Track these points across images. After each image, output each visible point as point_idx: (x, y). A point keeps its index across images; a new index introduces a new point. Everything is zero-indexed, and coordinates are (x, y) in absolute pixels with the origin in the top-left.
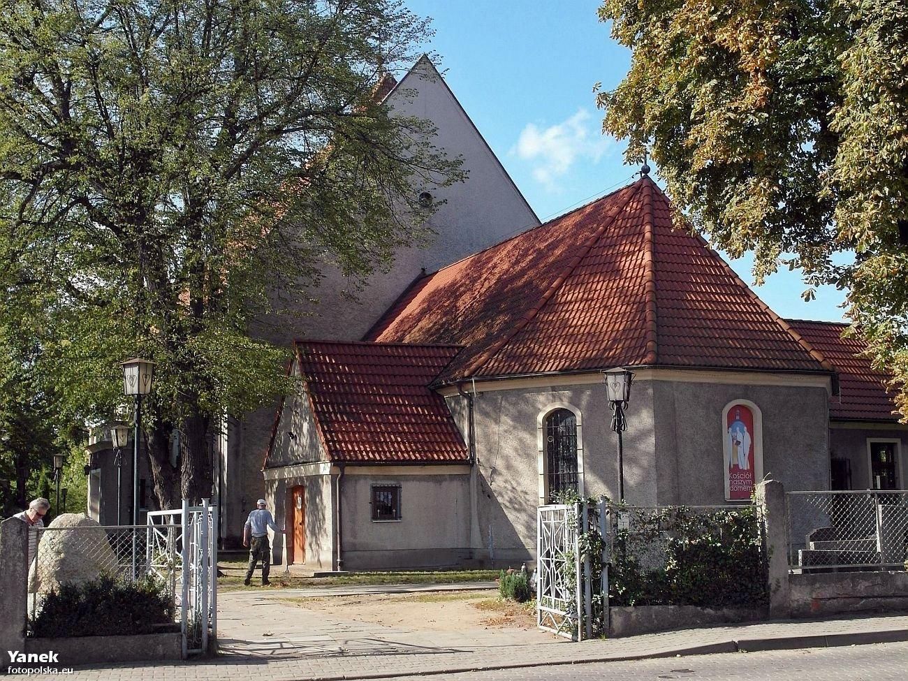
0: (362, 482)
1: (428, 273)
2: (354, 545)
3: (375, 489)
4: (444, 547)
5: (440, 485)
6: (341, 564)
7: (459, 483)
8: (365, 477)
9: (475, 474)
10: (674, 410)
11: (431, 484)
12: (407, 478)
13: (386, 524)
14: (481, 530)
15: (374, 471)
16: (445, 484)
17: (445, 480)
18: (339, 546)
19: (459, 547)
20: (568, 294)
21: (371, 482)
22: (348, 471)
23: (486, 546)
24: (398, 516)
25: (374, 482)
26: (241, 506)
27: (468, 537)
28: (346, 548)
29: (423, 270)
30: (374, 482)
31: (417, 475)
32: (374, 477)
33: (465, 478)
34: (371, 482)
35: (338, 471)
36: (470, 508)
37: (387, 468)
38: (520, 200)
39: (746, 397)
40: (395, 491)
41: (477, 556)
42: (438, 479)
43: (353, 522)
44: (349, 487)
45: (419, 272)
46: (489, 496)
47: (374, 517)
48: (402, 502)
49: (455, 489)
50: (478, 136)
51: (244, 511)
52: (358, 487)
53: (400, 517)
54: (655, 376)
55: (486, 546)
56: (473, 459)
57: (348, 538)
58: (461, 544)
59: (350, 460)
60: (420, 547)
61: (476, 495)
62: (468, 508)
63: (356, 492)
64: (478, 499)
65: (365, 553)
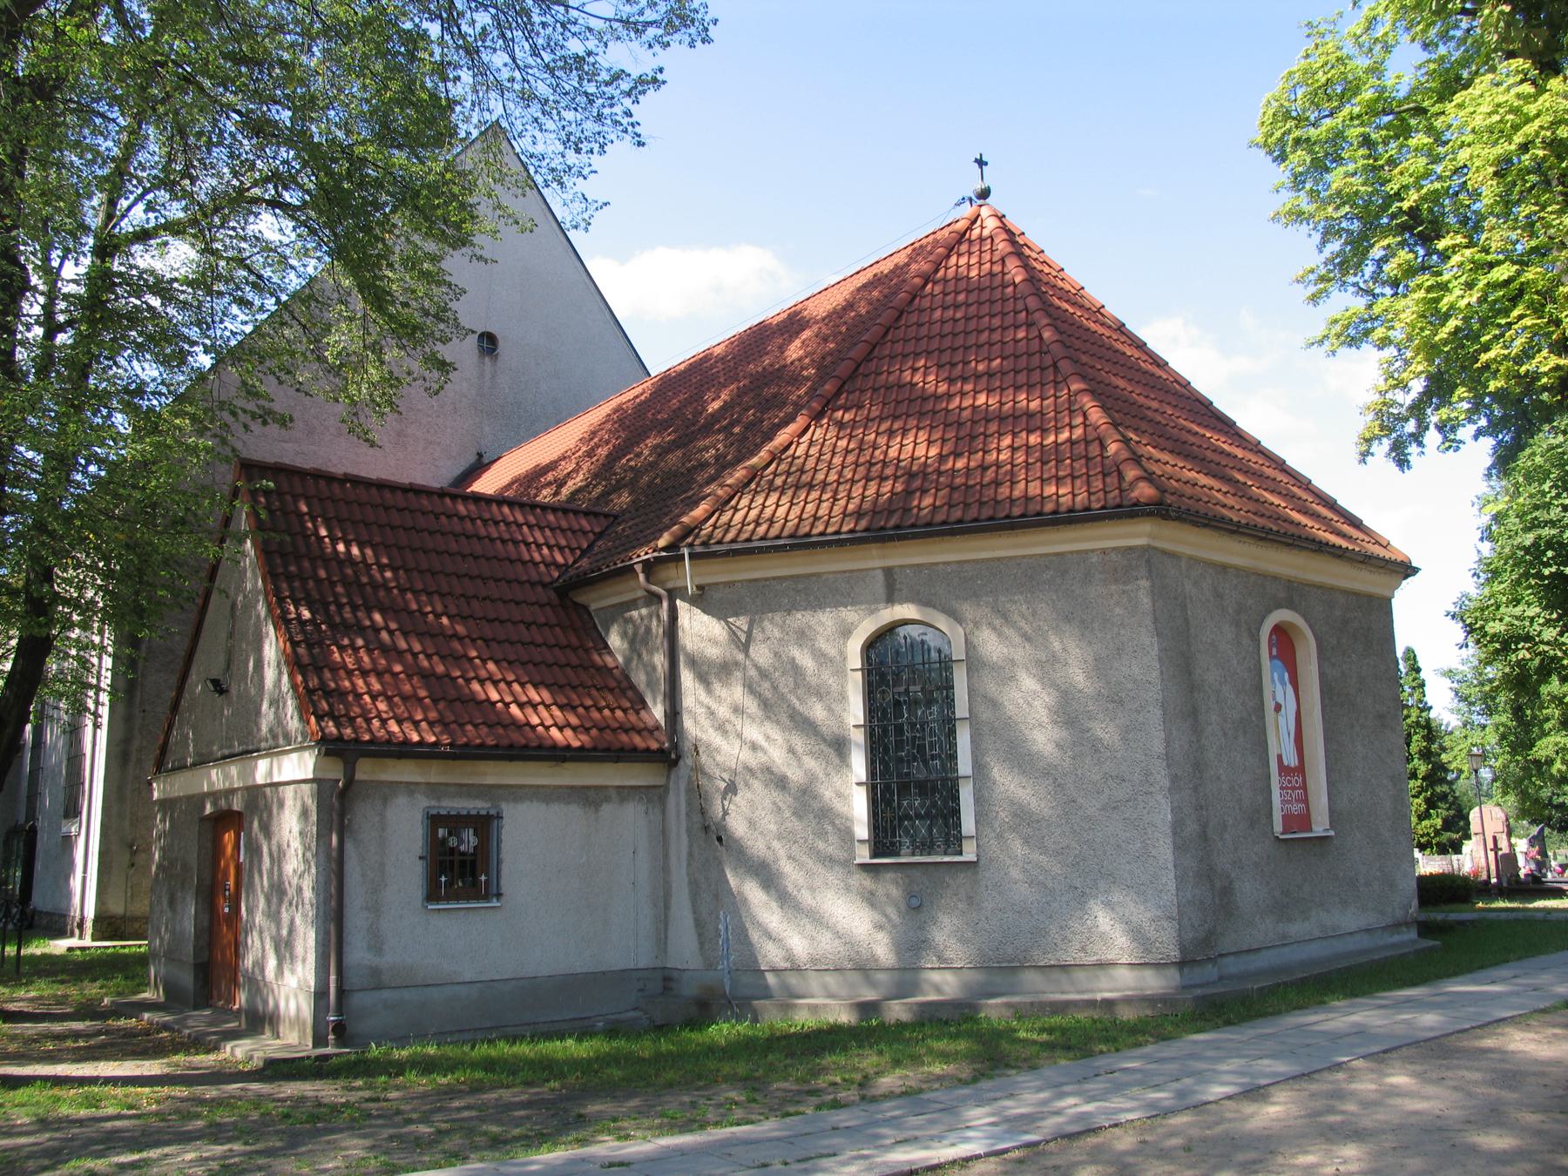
0: (401, 801)
1: (486, 460)
2: (375, 972)
3: (434, 820)
4: (603, 969)
5: (597, 811)
6: (339, 1029)
7: (641, 808)
8: (411, 788)
9: (683, 786)
10: (1187, 621)
11: (575, 811)
12: (517, 793)
13: (462, 913)
14: (699, 924)
15: (434, 773)
16: (607, 809)
17: (607, 799)
18: (333, 978)
19: (641, 966)
20: (799, 444)
21: (423, 802)
22: (366, 770)
23: (710, 965)
24: (490, 892)
25: (433, 803)
26: (127, 856)
27: (662, 940)
28: (353, 980)
29: (480, 455)
30: (433, 803)
31: (543, 786)
32: (433, 789)
33: (655, 796)
34: (423, 802)
35: (336, 772)
36: (666, 869)
37: (469, 766)
38: (636, 364)
39: (1290, 605)
40: (485, 824)
41: (689, 989)
42: (590, 797)
43: (375, 909)
44: (365, 815)
45: (472, 458)
46: (720, 839)
47: (433, 895)
48: (503, 855)
49: (630, 820)
50: (572, 255)
51: (133, 865)
52: (391, 814)
53: (499, 895)
54: (1154, 538)
55: (710, 965)
56: (675, 746)
57: (358, 953)
58: (644, 958)
59: (371, 742)
60: (545, 971)
61: (684, 837)
62: (663, 869)
63: (383, 830)
64: (690, 846)
65: (407, 995)
